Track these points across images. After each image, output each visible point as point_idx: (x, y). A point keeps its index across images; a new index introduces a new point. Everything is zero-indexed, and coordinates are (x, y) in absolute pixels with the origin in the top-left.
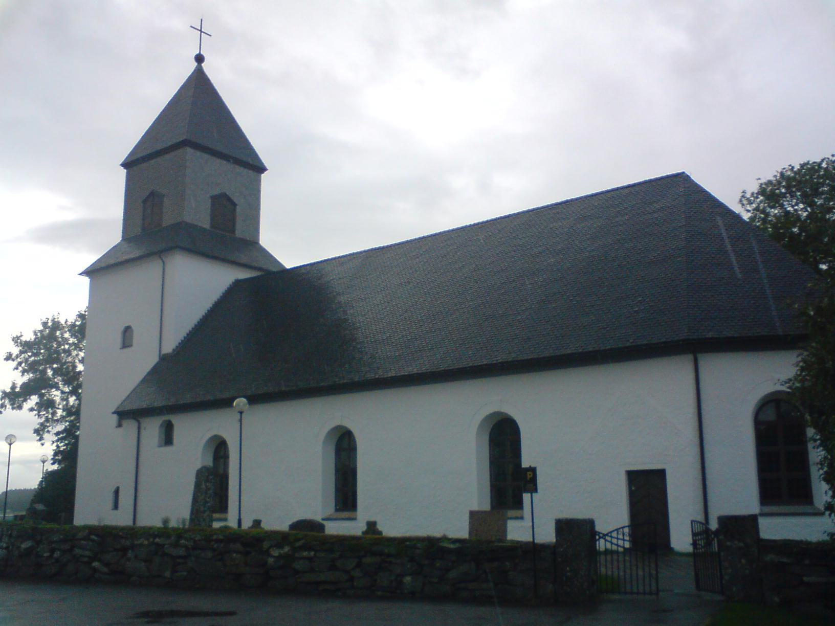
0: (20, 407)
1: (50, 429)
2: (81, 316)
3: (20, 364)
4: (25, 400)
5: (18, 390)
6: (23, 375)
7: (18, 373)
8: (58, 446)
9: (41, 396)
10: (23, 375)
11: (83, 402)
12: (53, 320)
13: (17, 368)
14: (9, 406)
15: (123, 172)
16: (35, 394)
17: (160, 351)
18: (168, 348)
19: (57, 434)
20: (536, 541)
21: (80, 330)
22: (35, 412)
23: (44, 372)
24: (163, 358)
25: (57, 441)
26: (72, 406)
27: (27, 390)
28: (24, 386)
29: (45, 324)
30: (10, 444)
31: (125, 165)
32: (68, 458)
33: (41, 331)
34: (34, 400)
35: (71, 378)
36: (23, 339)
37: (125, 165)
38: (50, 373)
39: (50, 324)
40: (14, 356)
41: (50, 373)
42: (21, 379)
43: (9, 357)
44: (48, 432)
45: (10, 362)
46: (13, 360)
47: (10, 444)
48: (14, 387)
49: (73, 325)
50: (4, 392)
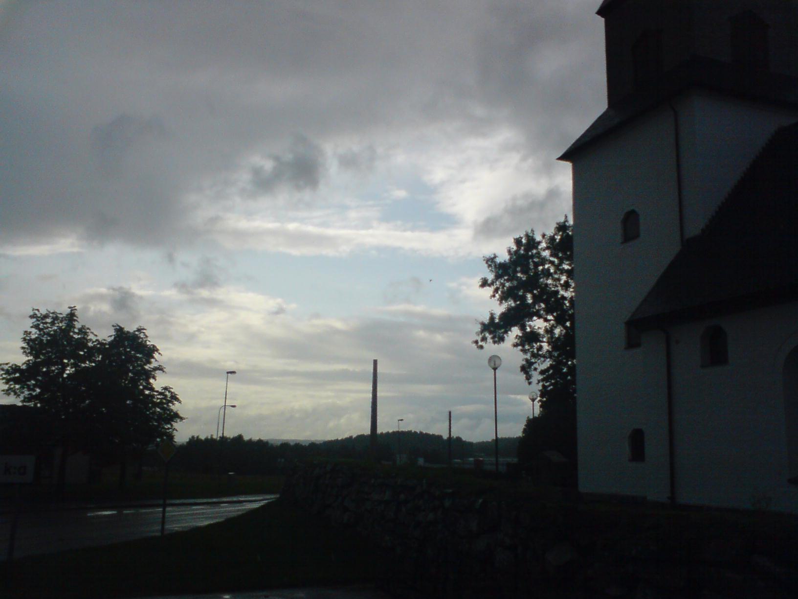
0: (502, 339)
1: (536, 365)
2: (562, 227)
3: (496, 290)
4: (506, 332)
5: (497, 321)
6: (501, 303)
7: (495, 301)
8: (544, 386)
9: (523, 328)
10: (501, 303)
11: (577, 325)
12: (527, 236)
13: (494, 296)
14: (490, 340)
15: (601, 21)
16: (514, 326)
17: (682, 235)
18: (694, 229)
19: (542, 372)
20: (499, 436)
21: (564, 244)
22: (520, 348)
23: (523, 298)
24: (689, 245)
25: (543, 380)
26: (558, 338)
27: (509, 319)
28: (503, 316)
29: (518, 242)
30: (495, 369)
31: (600, 12)
32: (559, 396)
33: (516, 252)
34: (515, 332)
35: (553, 304)
36: (498, 260)
37: (600, 12)
38: (529, 299)
39: (524, 241)
40: (489, 282)
41: (529, 299)
42: (499, 309)
43: (485, 283)
44: (535, 369)
45: (487, 288)
46: (489, 285)
47: (495, 369)
48: (492, 318)
49: (552, 239)
50: (483, 324)
